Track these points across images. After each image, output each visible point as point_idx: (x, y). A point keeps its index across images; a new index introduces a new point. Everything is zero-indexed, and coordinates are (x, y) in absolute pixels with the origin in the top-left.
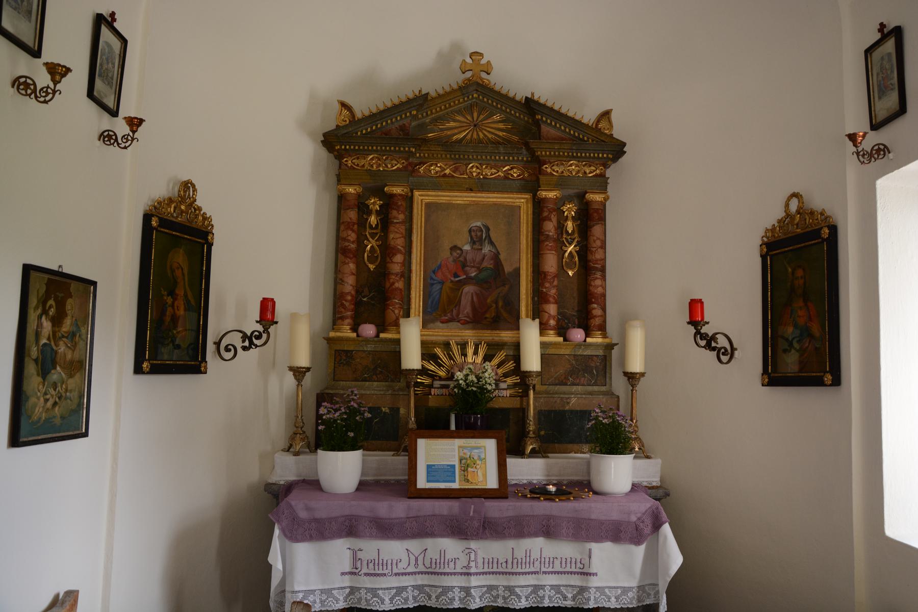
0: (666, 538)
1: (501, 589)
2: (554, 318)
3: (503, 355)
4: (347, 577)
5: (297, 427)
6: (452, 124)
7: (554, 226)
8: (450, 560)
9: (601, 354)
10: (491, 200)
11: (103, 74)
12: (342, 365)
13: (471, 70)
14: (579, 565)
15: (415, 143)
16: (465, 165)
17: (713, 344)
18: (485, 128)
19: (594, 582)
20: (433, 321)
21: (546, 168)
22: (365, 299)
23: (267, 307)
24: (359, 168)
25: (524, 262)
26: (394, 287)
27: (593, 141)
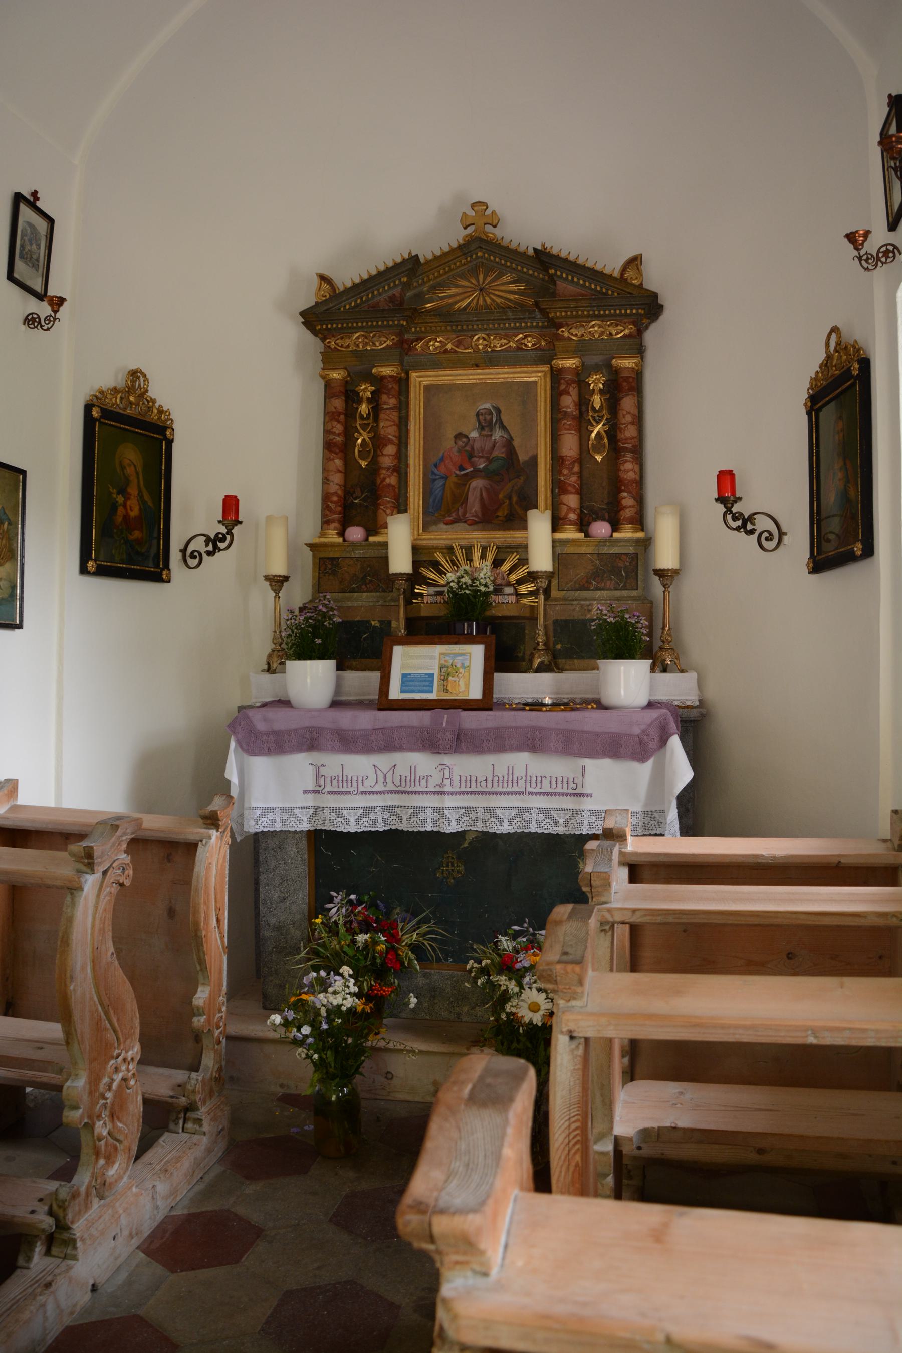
0: (673, 752)
1: (480, 812)
3: (516, 558)
4: (310, 796)
5: (275, 644)
7: (573, 401)
8: (422, 777)
9: (630, 552)
10: (539, 369)
11: (25, 256)
12: (327, 575)
13: (473, 224)
14: (571, 785)
15: (405, 314)
16: (470, 337)
17: (749, 527)
18: (493, 291)
19: (588, 805)
20: (435, 523)
21: (562, 331)
22: (356, 501)
23: (231, 505)
24: (344, 349)
25: (543, 448)
26: (385, 483)
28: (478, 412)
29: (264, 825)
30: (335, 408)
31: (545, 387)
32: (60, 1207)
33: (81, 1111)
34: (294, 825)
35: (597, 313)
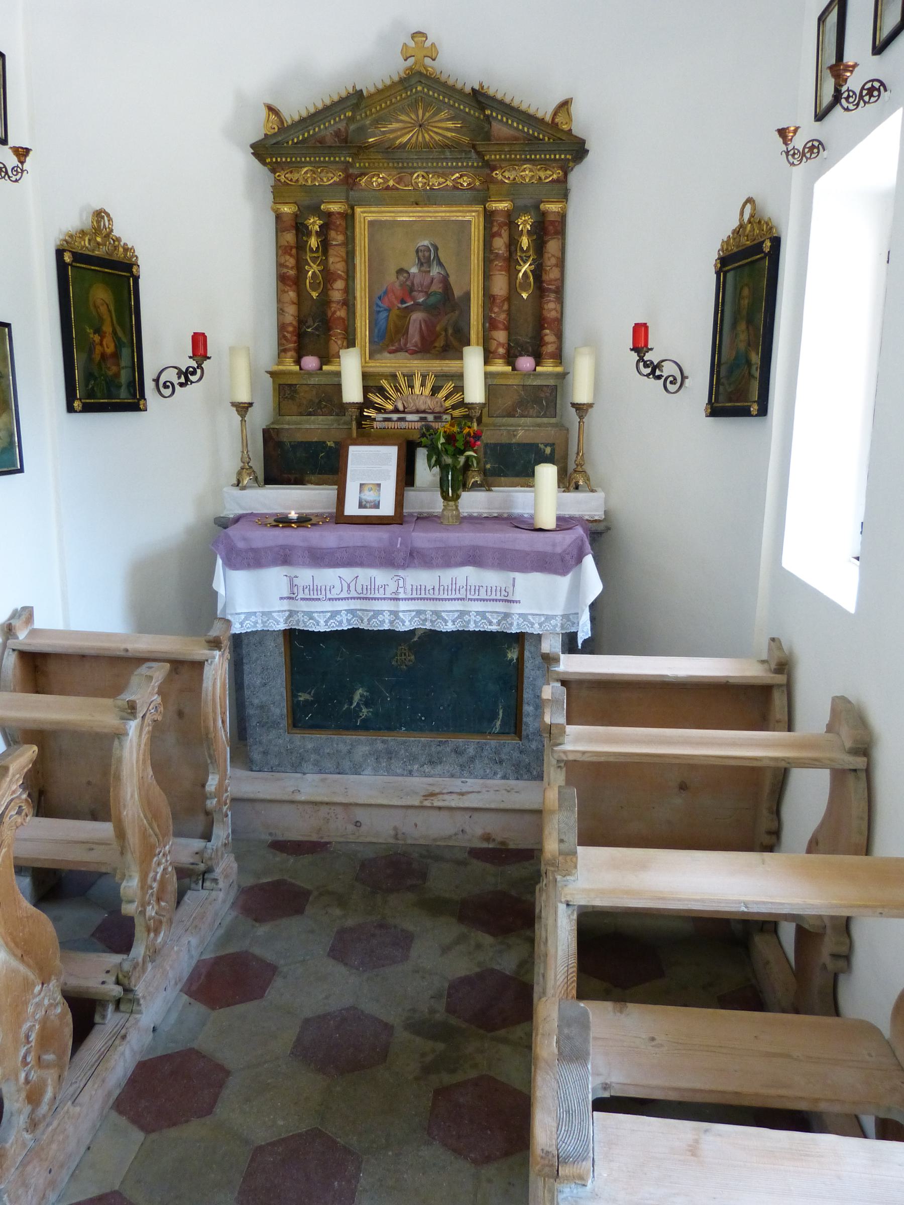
2: (503, 346)
5: (244, 463)
6: (395, 125)
8: (380, 586)
10: (474, 209)
14: (503, 593)
16: (410, 174)
17: (658, 373)
18: (431, 128)
19: (516, 609)
20: (380, 351)
21: (496, 174)
22: (309, 330)
23: (199, 342)
24: (293, 183)
26: (335, 316)
27: (549, 139)
28: (418, 249)
29: (248, 627)
30: (288, 242)
31: (479, 226)
32: (125, 977)
33: (136, 903)
34: (273, 625)
35: (528, 157)
